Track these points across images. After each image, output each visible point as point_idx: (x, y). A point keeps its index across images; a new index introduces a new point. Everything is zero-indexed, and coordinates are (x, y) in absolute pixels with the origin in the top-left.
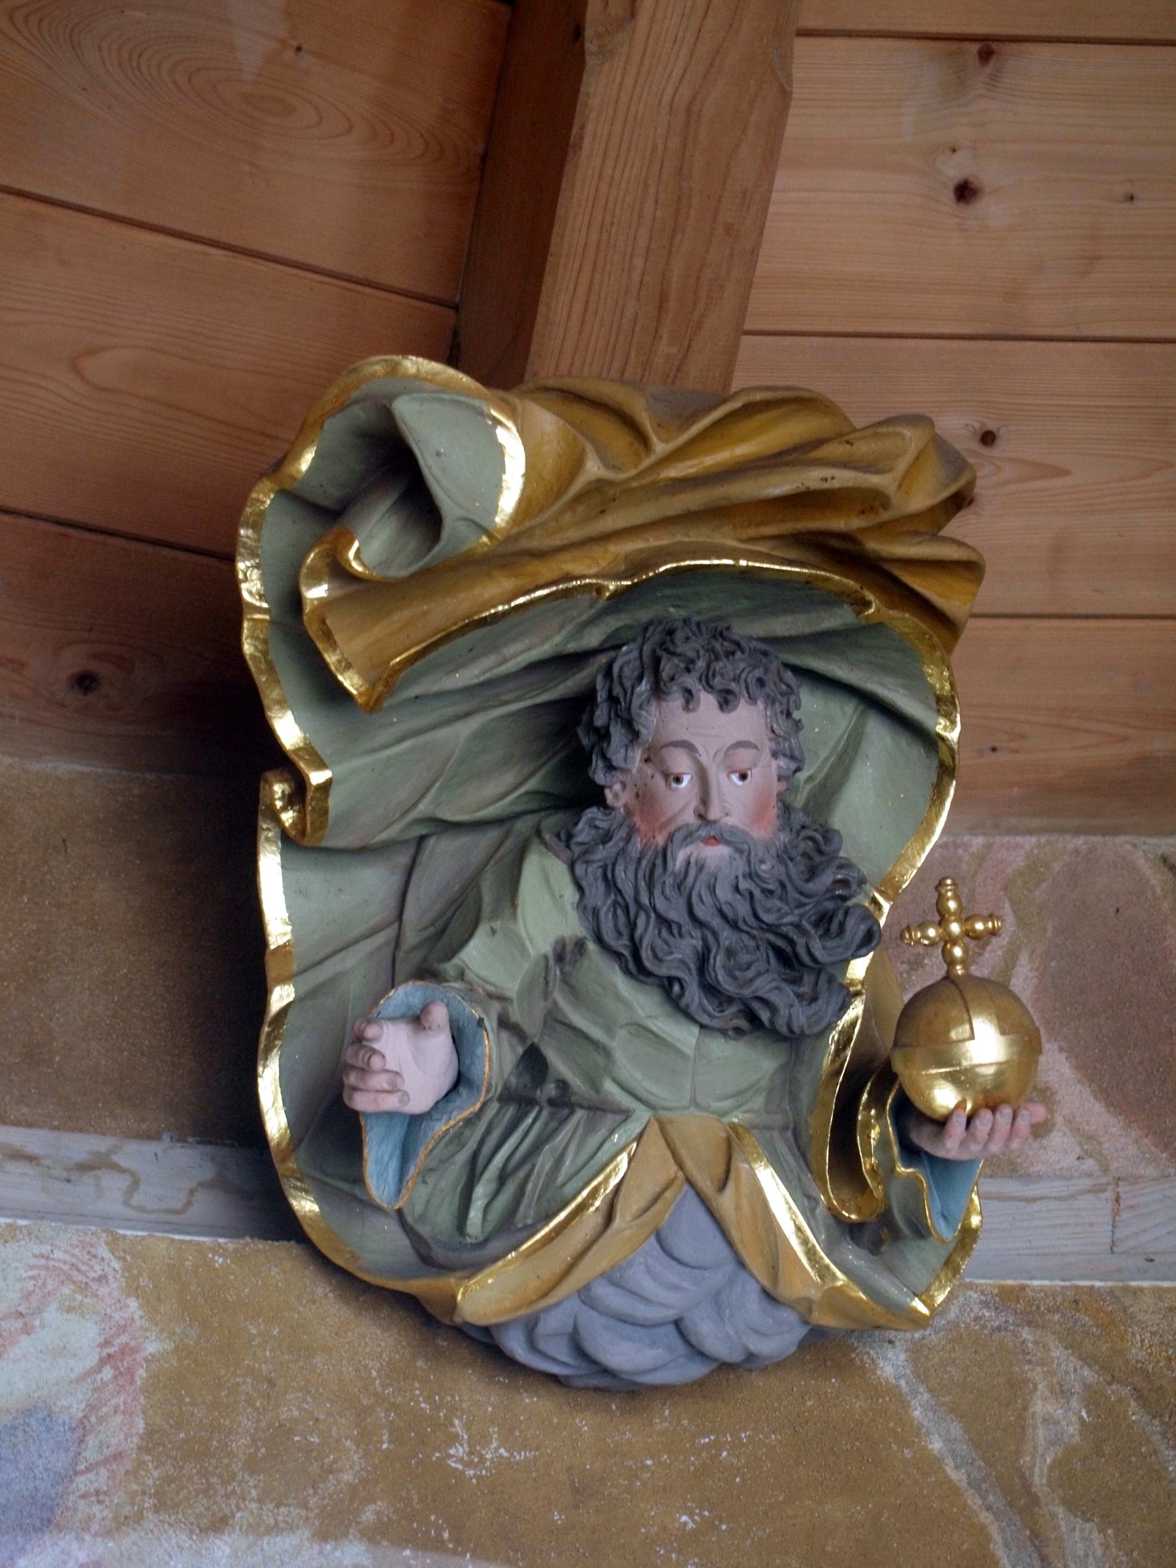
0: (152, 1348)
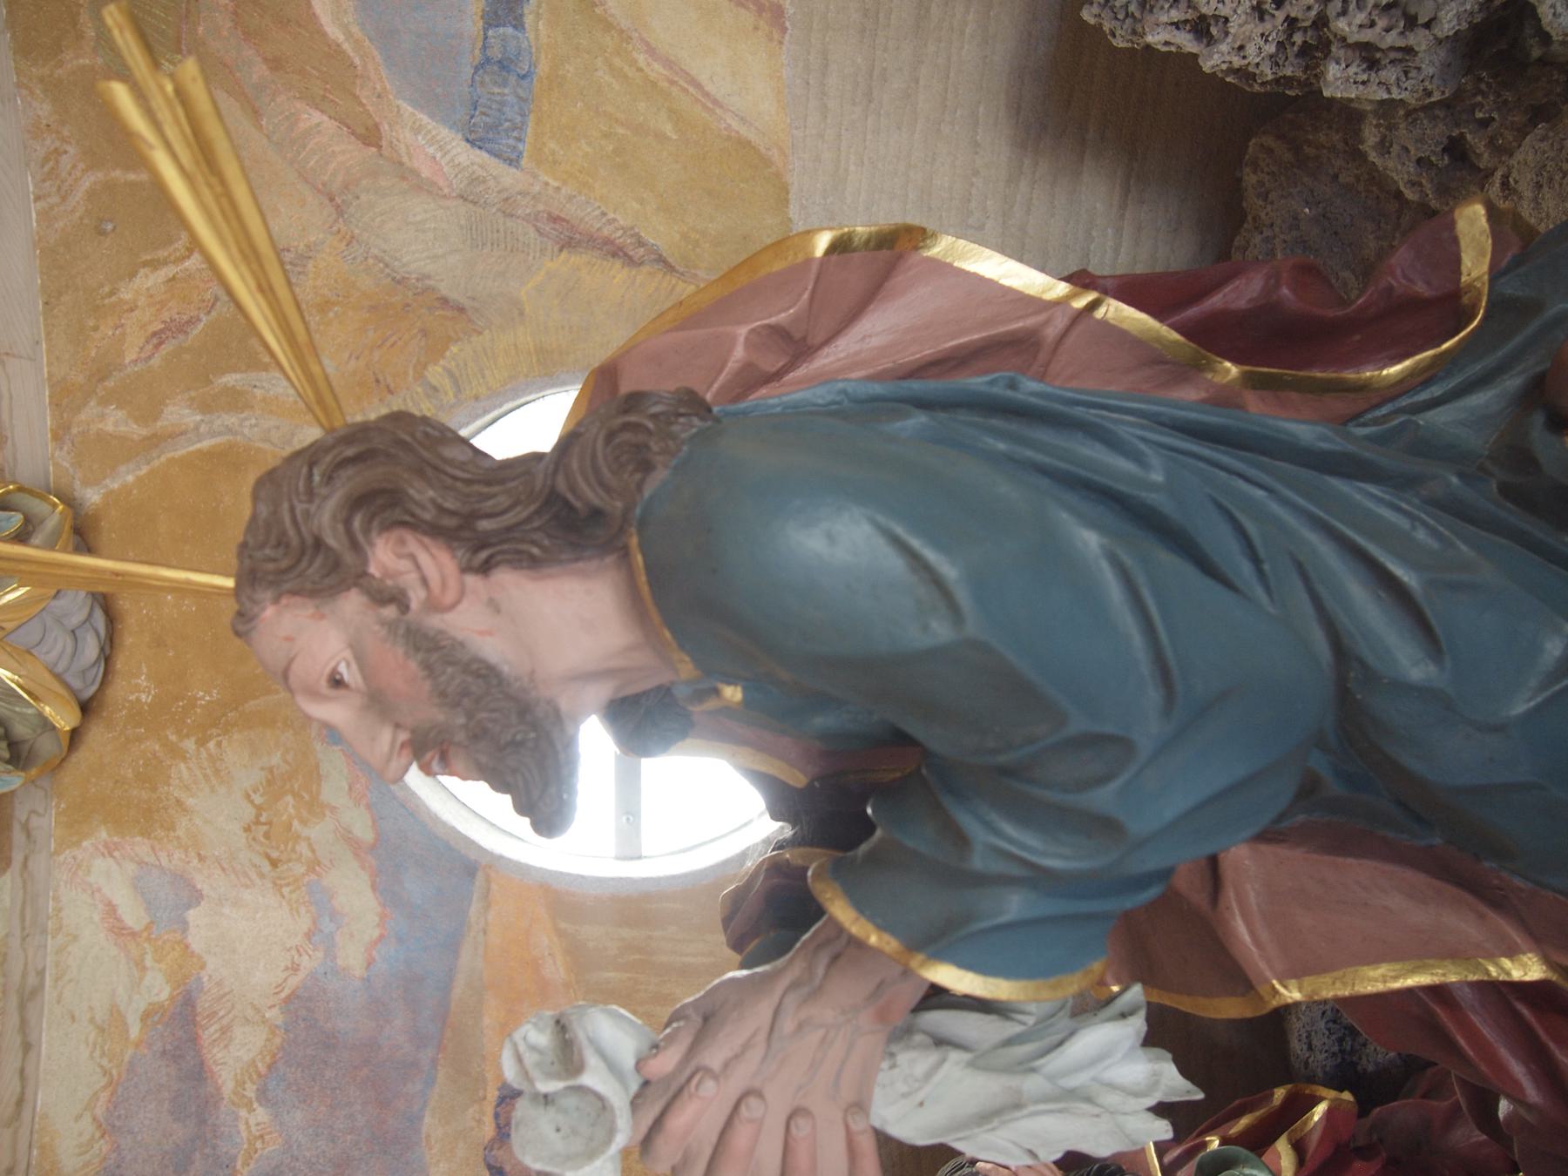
0: (104, 835)
